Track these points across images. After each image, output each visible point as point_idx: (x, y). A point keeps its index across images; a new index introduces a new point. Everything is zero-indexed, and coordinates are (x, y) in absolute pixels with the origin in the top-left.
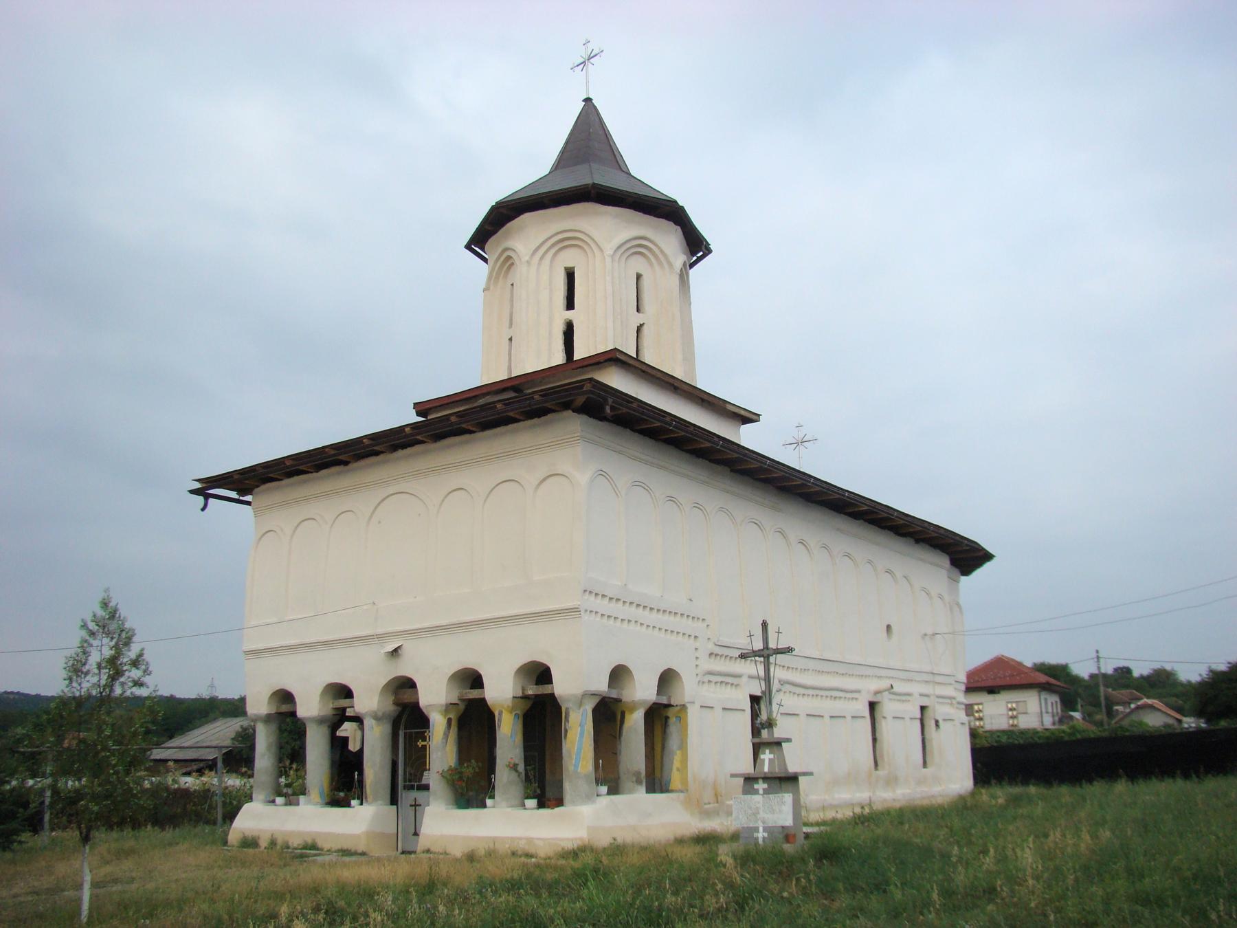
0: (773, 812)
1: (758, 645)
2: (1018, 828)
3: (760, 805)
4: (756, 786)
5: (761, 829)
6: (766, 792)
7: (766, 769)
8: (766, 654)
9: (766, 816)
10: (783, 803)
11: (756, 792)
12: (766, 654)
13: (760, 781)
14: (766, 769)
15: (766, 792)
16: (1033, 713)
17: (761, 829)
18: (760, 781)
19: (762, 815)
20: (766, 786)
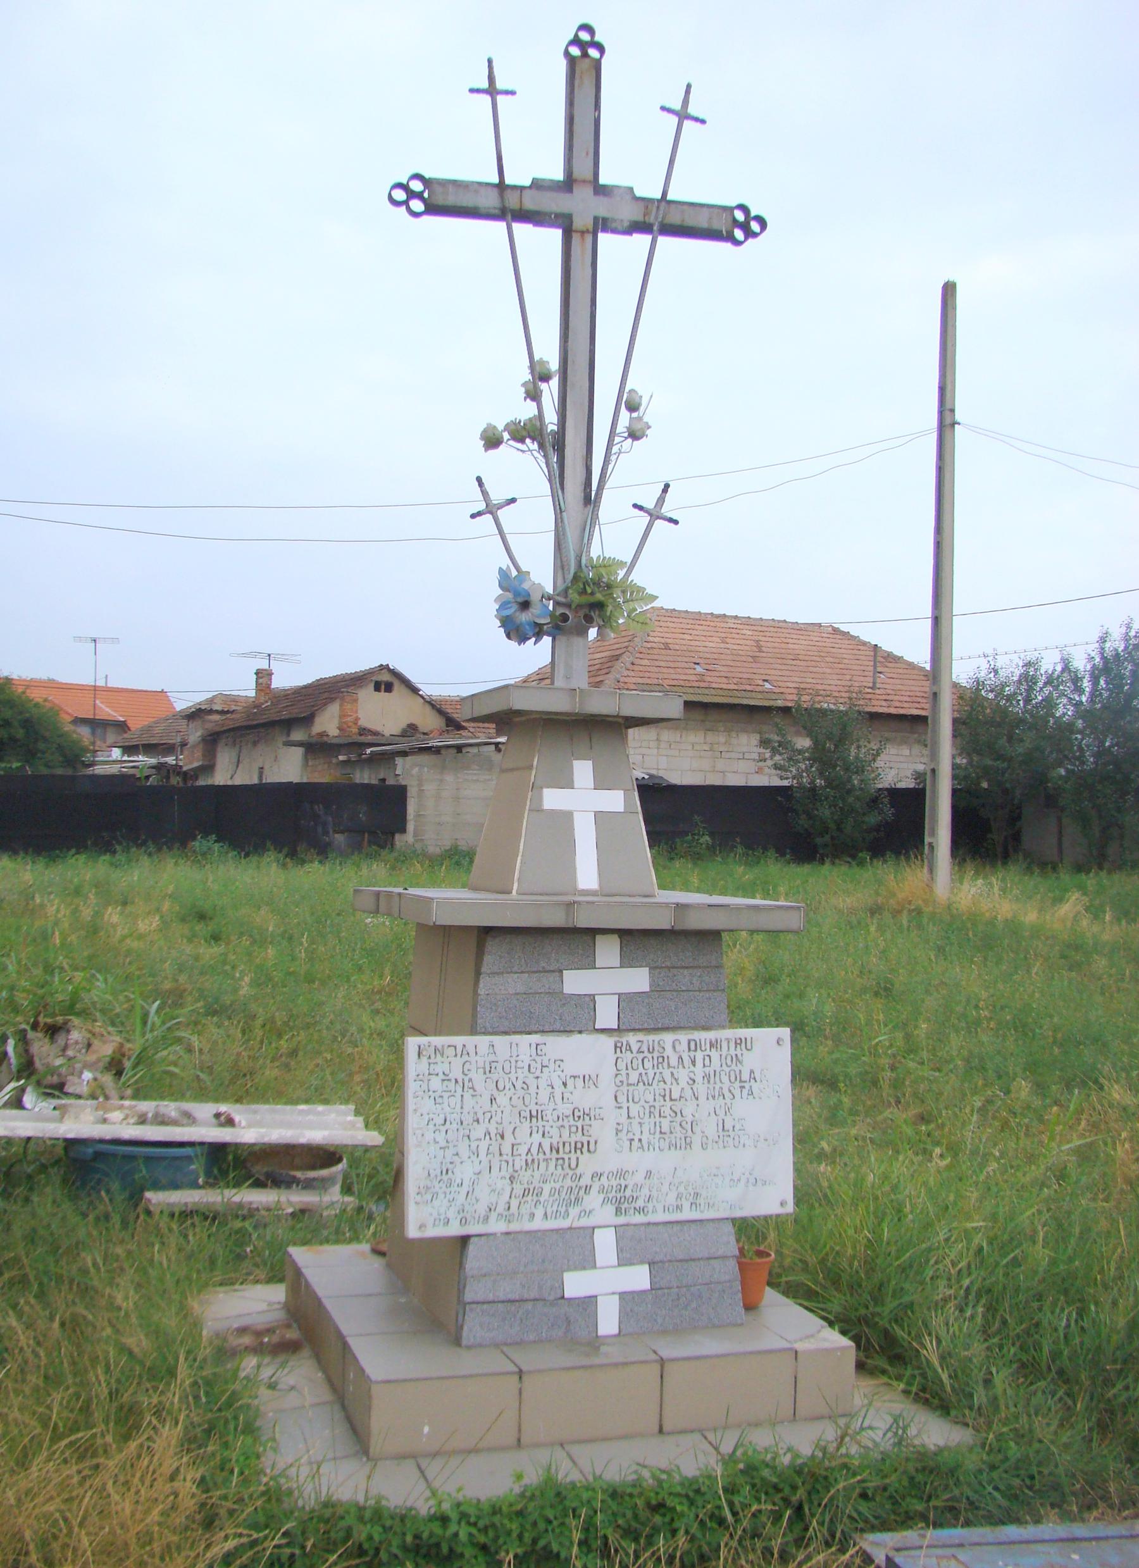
0: (683, 1138)
1: (537, 157)
2: (129, 1253)
3: (599, 1098)
4: (575, 982)
5: (605, 1243)
6: (637, 1015)
7: (587, 877)
8: (574, 209)
9: (638, 1162)
10: (745, 1083)
11: (576, 1017)
12: (574, 209)
13: (608, 951)
14: (587, 877)
15: (637, 1015)
16: (738, 762)
17: (605, 1243)
18: (608, 951)
19: (609, 1156)
20: (638, 980)
